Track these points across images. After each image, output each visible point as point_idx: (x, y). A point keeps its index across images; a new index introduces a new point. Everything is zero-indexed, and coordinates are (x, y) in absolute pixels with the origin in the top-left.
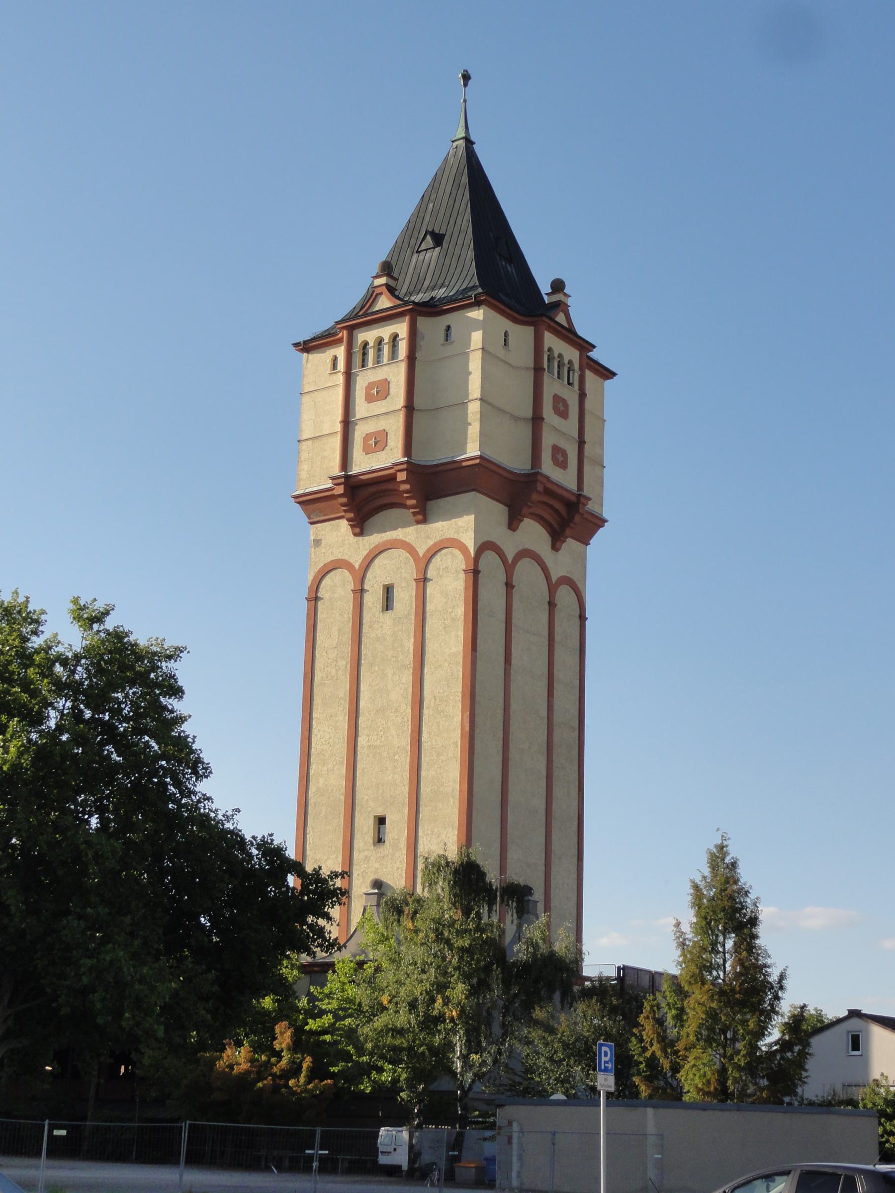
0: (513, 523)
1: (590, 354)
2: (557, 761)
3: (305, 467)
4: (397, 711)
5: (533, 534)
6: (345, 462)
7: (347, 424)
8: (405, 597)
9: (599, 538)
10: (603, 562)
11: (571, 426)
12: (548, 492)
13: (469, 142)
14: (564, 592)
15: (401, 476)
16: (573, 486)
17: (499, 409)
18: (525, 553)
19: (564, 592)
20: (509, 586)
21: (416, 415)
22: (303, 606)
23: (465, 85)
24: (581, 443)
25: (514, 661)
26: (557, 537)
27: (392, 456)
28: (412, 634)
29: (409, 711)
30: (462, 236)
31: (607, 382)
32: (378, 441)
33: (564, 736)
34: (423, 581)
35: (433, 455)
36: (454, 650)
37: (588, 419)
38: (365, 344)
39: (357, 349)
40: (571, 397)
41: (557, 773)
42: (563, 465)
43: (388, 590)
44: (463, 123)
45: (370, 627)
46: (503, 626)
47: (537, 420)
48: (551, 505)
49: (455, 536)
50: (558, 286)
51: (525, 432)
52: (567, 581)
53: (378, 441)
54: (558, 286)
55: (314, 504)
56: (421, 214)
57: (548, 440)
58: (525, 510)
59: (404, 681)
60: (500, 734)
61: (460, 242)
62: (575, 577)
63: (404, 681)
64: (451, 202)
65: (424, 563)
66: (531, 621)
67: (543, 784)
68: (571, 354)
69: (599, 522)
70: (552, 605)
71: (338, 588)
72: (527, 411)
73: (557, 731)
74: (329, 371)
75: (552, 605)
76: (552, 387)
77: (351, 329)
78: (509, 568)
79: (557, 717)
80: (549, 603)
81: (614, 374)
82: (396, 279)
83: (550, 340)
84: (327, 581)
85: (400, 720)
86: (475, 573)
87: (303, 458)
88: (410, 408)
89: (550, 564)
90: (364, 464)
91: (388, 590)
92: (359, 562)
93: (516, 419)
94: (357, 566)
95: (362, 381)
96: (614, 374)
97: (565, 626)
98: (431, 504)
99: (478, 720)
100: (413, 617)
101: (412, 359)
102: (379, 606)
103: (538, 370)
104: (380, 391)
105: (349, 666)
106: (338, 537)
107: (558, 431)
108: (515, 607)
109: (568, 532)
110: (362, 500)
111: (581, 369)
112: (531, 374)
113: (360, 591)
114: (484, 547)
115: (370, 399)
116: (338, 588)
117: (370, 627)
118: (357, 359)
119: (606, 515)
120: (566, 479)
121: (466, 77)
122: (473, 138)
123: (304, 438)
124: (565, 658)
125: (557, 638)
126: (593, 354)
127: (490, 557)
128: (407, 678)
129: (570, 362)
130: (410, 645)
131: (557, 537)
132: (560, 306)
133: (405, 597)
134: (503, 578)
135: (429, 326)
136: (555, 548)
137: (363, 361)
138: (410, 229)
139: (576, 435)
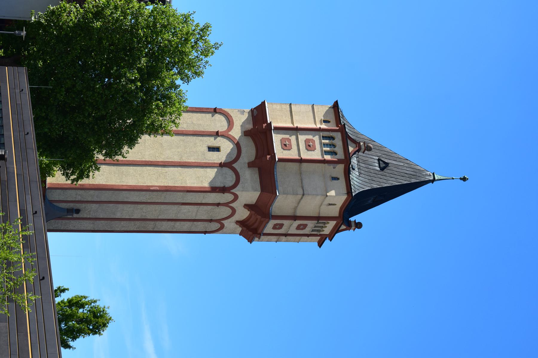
0: (247, 206)
1: (328, 239)
3: (278, 107)
4: (161, 153)
5: (243, 214)
6: (277, 129)
7: (296, 130)
9: (243, 240)
10: (233, 241)
11: (293, 231)
12: (261, 222)
16: (266, 231)
17: (299, 202)
18: (234, 211)
20: (218, 205)
21: (297, 164)
22: (212, 106)
23: (461, 179)
24: (286, 235)
25: (184, 206)
26: (240, 223)
27: (279, 153)
28: (197, 161)
29: (161, 160)
30: (385, 181)
31: (317, 243)
32: (285, 146)
33: (150, 225)
36: (188, 182)
37: (298, 238)
39: (331, 134)
40: (307, 231)
41: (133, 223)
42: (275, 227)
43: (217, 149)
44: (442, 178)
45: (201, 140)
46: (200, 202)
47: (295, 218)
49: (241, 182)
50: (359, 225)
51: (289, 212)
52: (222, 227)
55: (259, 114)
56: (398, 160)
57: (286, 223)
58: (253, 212)
59: (175, 157)
60: (149, 201)
61: (381, 180)
62: (224, 230)
63: (175, 157)
64: (403, 174)
67: (127, 217)
68: (327, 230)
69: (250, 241)
70: (211, 221)
71: (219, 123)
72: (298, 214)
73: (152, 223)
75: (211, 221)
76: (311, 224)
78: (226, 205)
79: (158, 223)
80: (212, 220)
81: (320, 247)
82: (363, 153)
83: (331, 224)
84: (222, 118)
85: (157, 155)
87: (283, 106)
88: (301, 161)
89: (229, 220)
90: (277, 138)
91: (217, 149)
93: (296, 208)
94: (230, 133)
96: (320, 247)
97: (201, 226)
99: (154, 193)
100: (204, 161)
101: (324, 162)
103: (318, 218)
104: (309, 147)
105: (183, 129)
107: (291, 226)
108: (209, 207)
109: (245, 229)
111: (320, 235)
112: (316, 215)
113: (217, 134)
116: (219, 123)
117: (201, 140)
118: (326, 134)
119: (253, 243)
120: (269, 228)
121: (464, 179)
122: (435, 182)
123: (292, 106)
124: (186, 226)
125: (195, 223)
126: (327, 241)
128: (176, 159)
129: (324, 231)
130: (192, 160)
131: (240, 223)
132: (349, 226)
134: (221, 202)
136: (238, 222)
137: (326, 137)
138: (390, 154)
139: (289, 232)
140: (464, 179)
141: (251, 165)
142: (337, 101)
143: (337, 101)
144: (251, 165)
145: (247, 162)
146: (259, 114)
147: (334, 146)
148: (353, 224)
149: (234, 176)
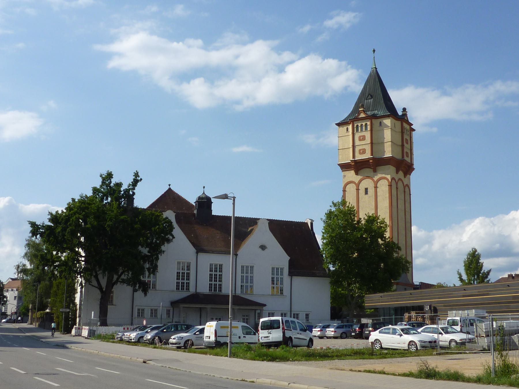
0: (397, 172)
2: (407, 231)
5: (401, 174)
6: (354, 156)
7: (354, 146)
8: (371, 191)
10: (414, 178)
13: (376, 68)
14: (407, 188)
15: (371, 161)
16: (410, 162)
19: (407, 188)
21: (374, 146)
27: (367, 155)
32: (363, 152)
34: (376, 187)
35: (377, 156)
38: (357, 126)
43: (366, 189)
47: (403, 146)
48: (404, 166)
53: (363, 152)
54: (404, 110)
55: (345, 167)
65: (376, 183)
66: (401, 197)
70: (405, 192)
75: (405, 192)
77: (353, 122)
78: (397, 184)
83: (405, 125)
86: (390, 186)
88: (372, 143)
91: (366, 189)
93: (397, 145)
95: (357, 136)
98: (378, 168)
101: (371, 130)
103: (402, 133)
104: (363, 138)
106: (351, 175)
110: (358, 166)
113: (358, 190)
114: (393, 179)
115: (360, 140)
121: (374, 51)
127: (393, 181)
130: (373, 203)
133: (371, 191)
135: (376, 122)
136: (405, 177)
148: (404, 113)
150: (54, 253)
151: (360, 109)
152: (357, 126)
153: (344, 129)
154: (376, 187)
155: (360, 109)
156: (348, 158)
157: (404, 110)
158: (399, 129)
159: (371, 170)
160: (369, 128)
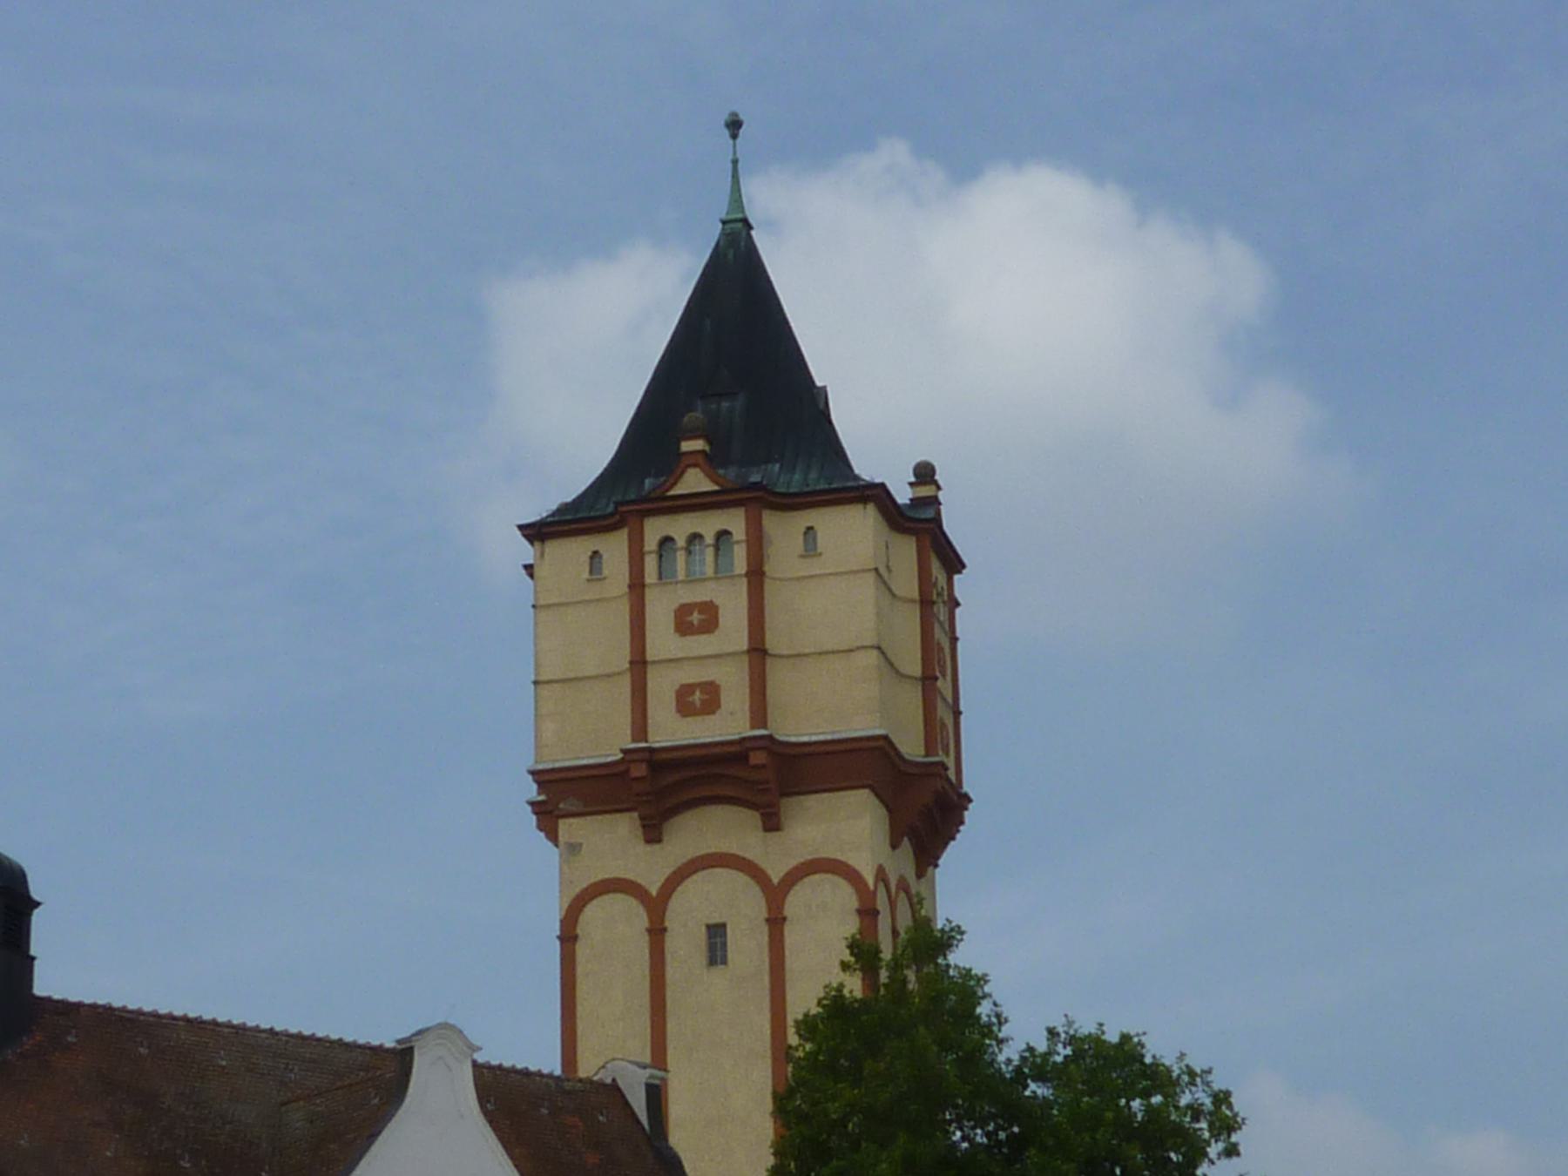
6: (640, 728)
7: (639, 663)
8: (748, 945)
23: (734, 136)
27: (728, 724)
34: (776, 922)
43: (717, 932)
49: (839, 856)
53: (698, 699)
54: (925, 474)
65: (775, 894)
74: (586, 575)
78: (775, 894)
88: (758, 652)
91: (717, 932)
92: (659, 884)
102: (701, 957)
104: (697, 620)
106: (612, 843)
110: (652, 787)
113: (657, 932)
115: (683, 626)
116: (615, 927)
118: (651, 564)
121: (734, 125)
140: (734, 125)
141: (772, 823)
142: (521, 527)
143: (521, 527)
144: (772, 823)
145: (761, 834)
146: (563, 795)
147: (695, 538)
148: (925, 491)
149: (619, 897)
150: (1016, 1129)
151: (686, 446)
152: (667, 541)
153: (577, 549)
154: (776, 922)
155: (686, 446)
156: (602, 739)
157: (925, 474)
158: (907, 582)
159: (752, 818)
160: (740, 558)
